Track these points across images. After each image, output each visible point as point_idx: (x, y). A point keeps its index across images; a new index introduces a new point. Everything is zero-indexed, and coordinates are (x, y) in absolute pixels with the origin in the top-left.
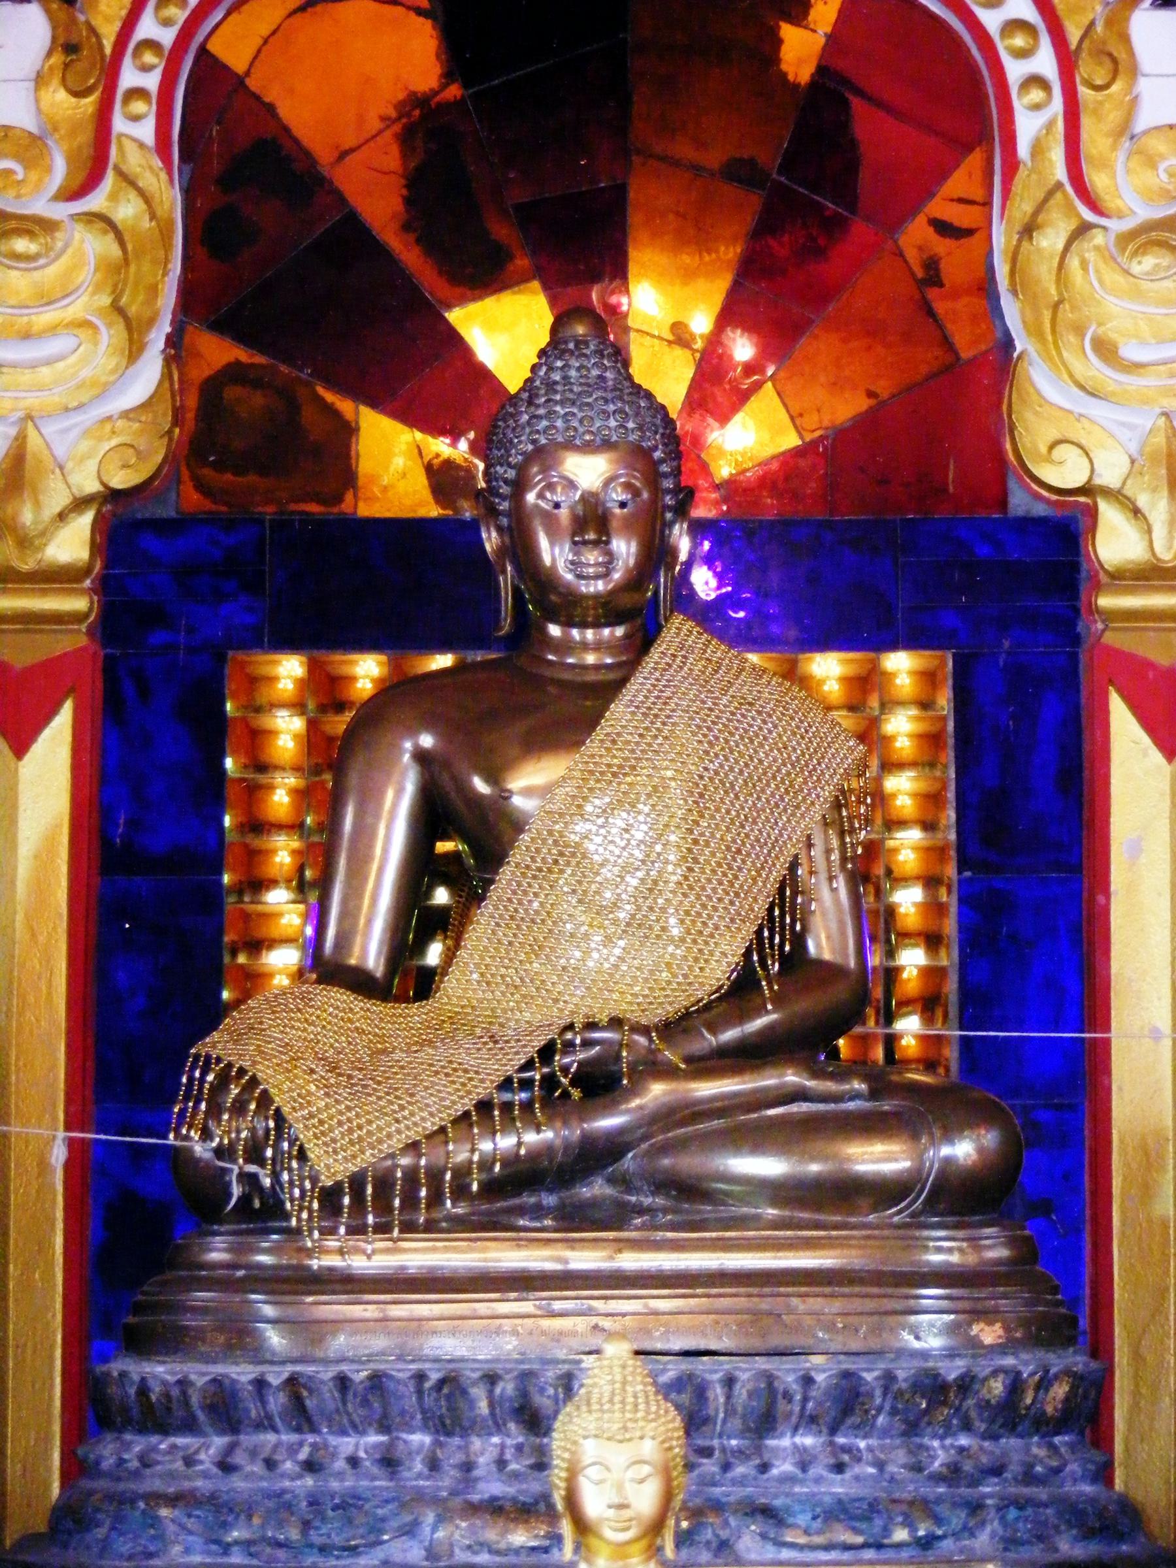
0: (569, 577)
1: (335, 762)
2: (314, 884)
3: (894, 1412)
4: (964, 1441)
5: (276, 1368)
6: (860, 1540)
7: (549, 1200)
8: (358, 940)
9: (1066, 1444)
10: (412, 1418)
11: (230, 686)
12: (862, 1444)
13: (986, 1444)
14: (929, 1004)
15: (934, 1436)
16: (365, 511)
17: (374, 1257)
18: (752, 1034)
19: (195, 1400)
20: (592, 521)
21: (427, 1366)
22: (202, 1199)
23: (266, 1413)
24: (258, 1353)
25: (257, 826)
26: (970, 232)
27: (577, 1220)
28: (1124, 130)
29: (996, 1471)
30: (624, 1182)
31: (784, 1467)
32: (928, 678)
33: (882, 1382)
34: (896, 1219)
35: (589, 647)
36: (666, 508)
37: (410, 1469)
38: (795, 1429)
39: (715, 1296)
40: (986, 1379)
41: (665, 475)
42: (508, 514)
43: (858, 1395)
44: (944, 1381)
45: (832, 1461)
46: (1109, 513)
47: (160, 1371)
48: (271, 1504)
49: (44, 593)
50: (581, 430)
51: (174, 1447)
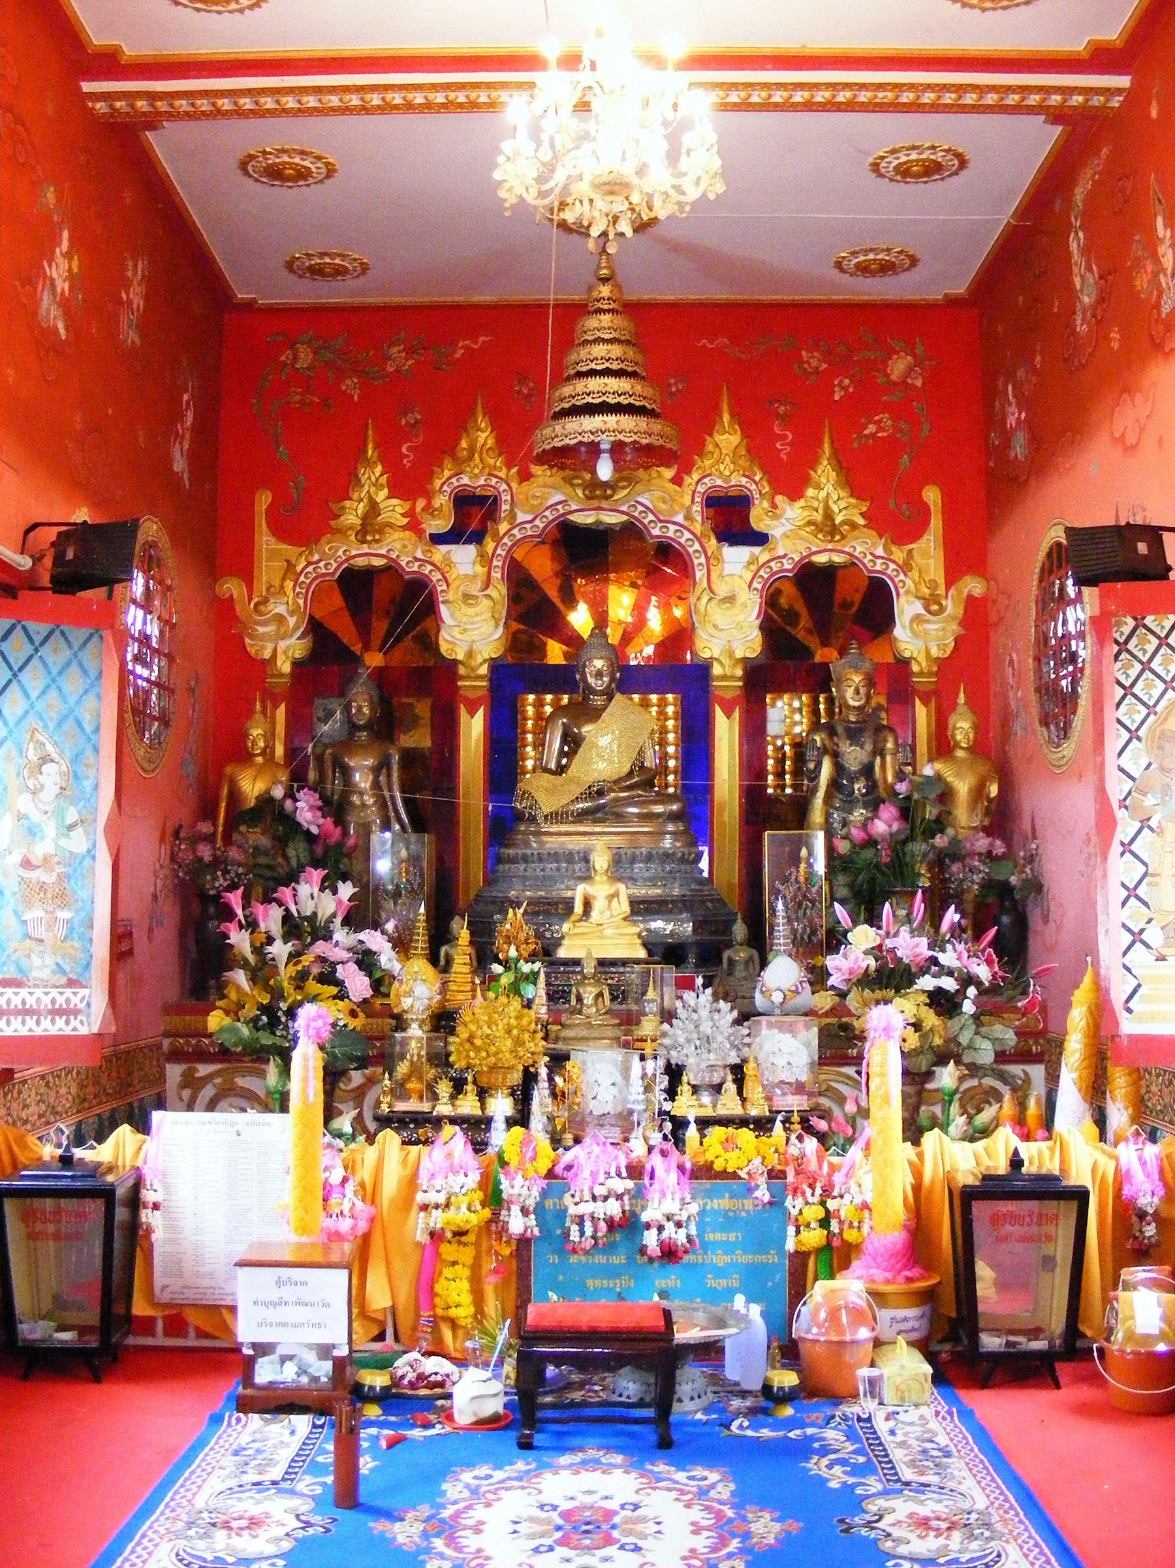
2: (539, 744)
14: (675, 773)
17: (554, 828)
20: (599, 674)
22: (519, 817)
24: (531, 847)
27: (596, 821)
28: (721, 576)
35: (598, 701)
46: (715, 664)
47: (511, 851)
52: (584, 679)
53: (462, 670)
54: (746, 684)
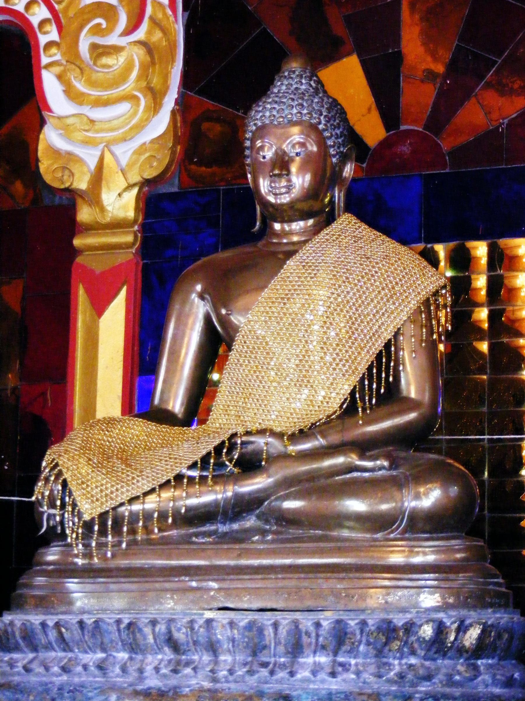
4: (413, 661)
10: (117, 644)
12: (353, 662)
13: (427, 663)
23: (48, 640)
29: (428, 678)
30: (264, 517)
31: (303, 674)
33: (358, 627)
37: (113, 671)
38: (315, 652)
40: (421, 626)
43: (346, 634)
44: (395, 626)
45: (330, 671)
49: (114, 234)
50: (277, 116)
53: (85, 214)
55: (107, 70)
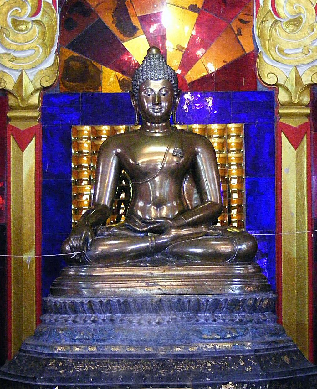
0: (152, 112)
1: (99, 153)
3: (227, 308)
5: (85, 299)
6: (219, 337)
7: (148, 259)
8: (103, 198)
9: (268, 314)
11: (72, 133)
12: (220, 315)
15: (236, 313)
16: (104, 91)
17: (107, 272)
18: (195, 219)
19: (67, 307)
20: (157, 101)
21: (120, 298)
25: (80, 167)
26: (248, 22)
27: (154, 263)
29: (251, 321)
30: (166, 255)
32: (239, 129)
33: (224, 301)
34: (228, 263)
36: (175, 95)
39: (187, 281)
41: (174, 87)
42: (137, 97)
45: (213, 319)
47: (60, 300)
48: (85, 330)
51: (63, 317)
52: (140, 104)
53: (12, 101)
54: (313, 111)
55: (24, 33)
